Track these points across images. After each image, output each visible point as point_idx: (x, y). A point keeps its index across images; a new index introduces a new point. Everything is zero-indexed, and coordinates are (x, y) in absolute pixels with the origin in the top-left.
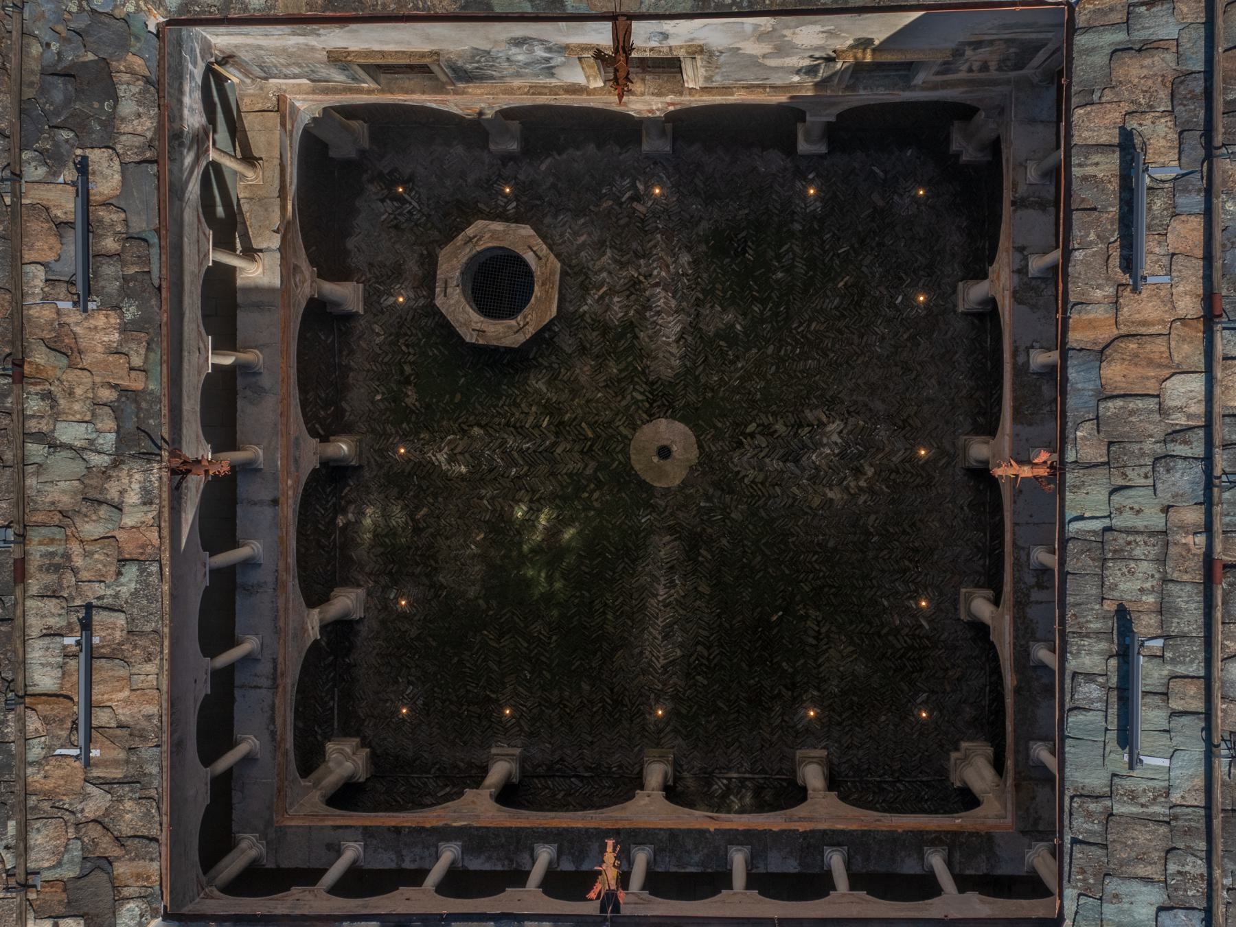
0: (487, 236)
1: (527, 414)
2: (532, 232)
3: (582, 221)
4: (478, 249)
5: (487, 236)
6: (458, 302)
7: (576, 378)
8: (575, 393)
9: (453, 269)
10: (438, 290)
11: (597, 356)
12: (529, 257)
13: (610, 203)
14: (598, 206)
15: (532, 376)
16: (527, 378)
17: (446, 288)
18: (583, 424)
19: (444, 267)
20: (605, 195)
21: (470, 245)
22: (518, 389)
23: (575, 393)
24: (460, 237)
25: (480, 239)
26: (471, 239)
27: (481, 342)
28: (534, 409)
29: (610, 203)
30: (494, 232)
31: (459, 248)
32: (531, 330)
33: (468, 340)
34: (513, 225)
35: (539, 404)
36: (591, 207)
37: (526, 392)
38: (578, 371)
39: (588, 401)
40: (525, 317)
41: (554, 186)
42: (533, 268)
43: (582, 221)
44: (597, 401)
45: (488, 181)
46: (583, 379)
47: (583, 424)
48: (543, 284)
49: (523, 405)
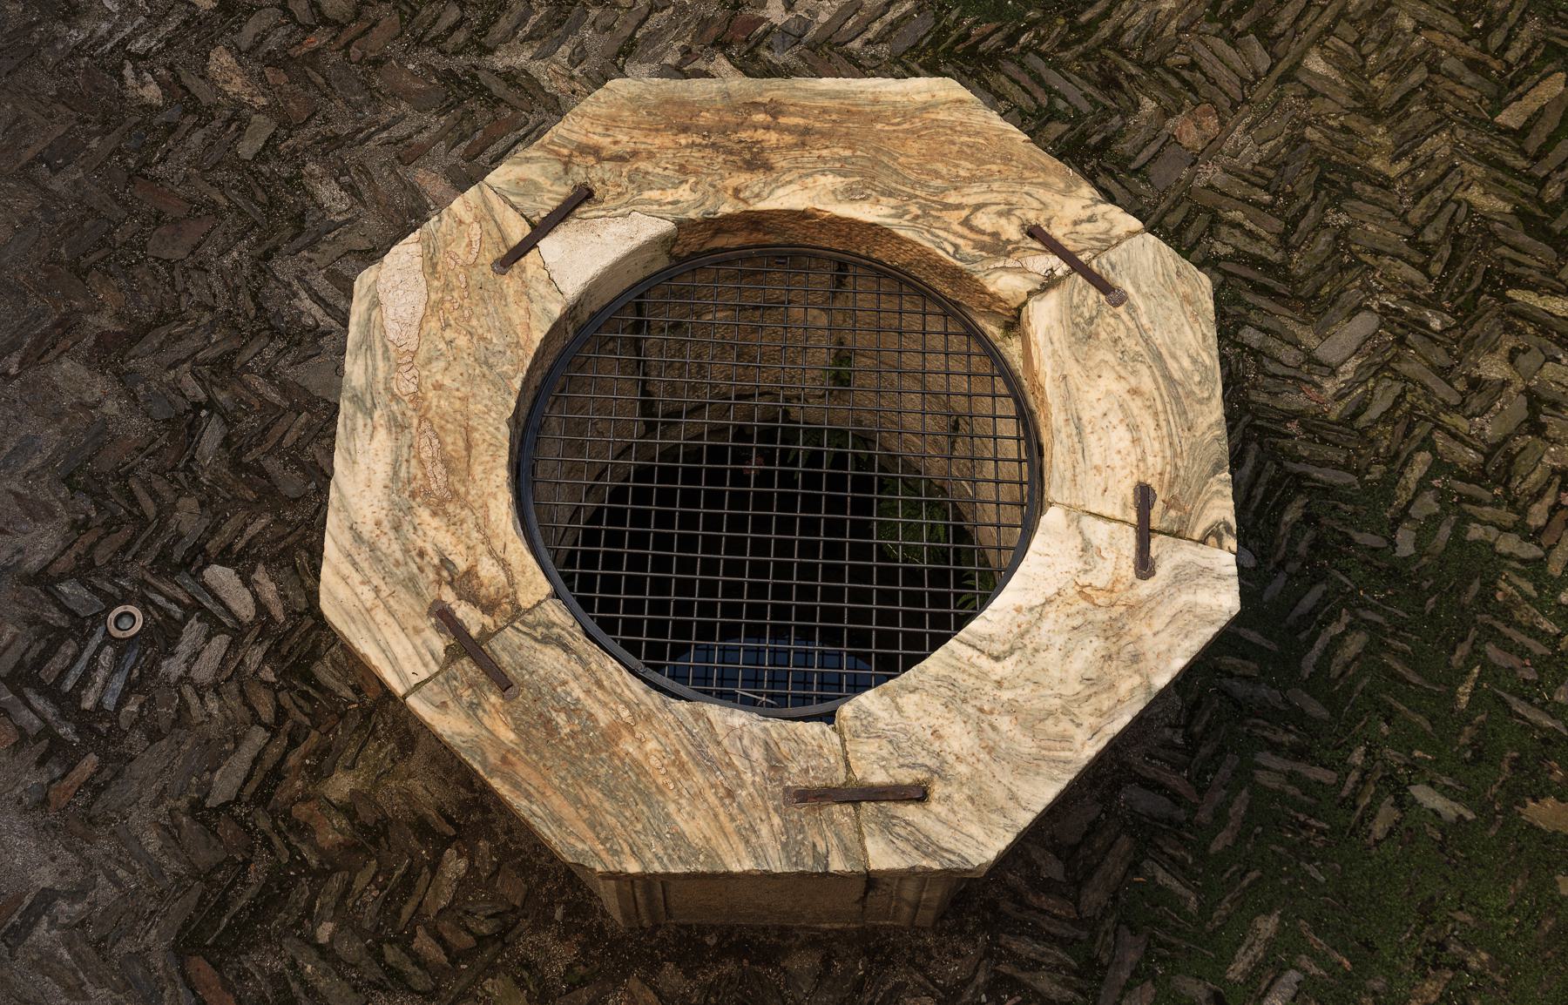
0: (434, 533)
1: (1534, 399)
2: (405, 254)
3: (329, 194)
4: (534, 585)
5: (434, 533)
6: (955, 696)
7: (1254, 178)
8: (1337, 179)
9: (704, 755)
10: (882, 856)
11: (1109, 83)
12: (580, 259)
13: (221, 60)
14: (238, 117)
15: (1295, 400)
16: (1315, 426)
17: (858, 795)
18: (1510, 117)
19: (693, 825)
20: (173, 86)
21: (510, 647)
22: (1396, 462)
23: (1337, 179)
24: (449, 725)
25: (466, 584)
26: (465, 646)
27: (1222, 509)
28: (1493, 368)
29: (221, 60)
30: (407, 494)
31: (537, 728)
32: (1074, 208)
33: (1226, 601)
34: (355, 371)
35: (1460, 340)
36: (247, 148)
37: (1403, 417)
38: (1211, 173)
39: (1370, 109)
40: (997, 247)
41: (109, 353)
42: (648, 227)
43: (329, 194)
44: (1355, 70)
45: (55, 751)
46: (1248, 146)
47: (1510, 117)
48: (756, 161)
49: (1491, 430)
